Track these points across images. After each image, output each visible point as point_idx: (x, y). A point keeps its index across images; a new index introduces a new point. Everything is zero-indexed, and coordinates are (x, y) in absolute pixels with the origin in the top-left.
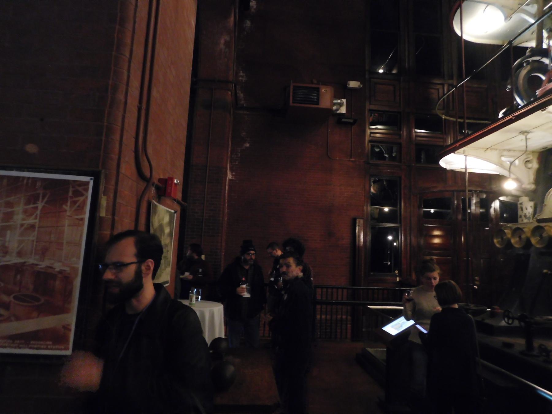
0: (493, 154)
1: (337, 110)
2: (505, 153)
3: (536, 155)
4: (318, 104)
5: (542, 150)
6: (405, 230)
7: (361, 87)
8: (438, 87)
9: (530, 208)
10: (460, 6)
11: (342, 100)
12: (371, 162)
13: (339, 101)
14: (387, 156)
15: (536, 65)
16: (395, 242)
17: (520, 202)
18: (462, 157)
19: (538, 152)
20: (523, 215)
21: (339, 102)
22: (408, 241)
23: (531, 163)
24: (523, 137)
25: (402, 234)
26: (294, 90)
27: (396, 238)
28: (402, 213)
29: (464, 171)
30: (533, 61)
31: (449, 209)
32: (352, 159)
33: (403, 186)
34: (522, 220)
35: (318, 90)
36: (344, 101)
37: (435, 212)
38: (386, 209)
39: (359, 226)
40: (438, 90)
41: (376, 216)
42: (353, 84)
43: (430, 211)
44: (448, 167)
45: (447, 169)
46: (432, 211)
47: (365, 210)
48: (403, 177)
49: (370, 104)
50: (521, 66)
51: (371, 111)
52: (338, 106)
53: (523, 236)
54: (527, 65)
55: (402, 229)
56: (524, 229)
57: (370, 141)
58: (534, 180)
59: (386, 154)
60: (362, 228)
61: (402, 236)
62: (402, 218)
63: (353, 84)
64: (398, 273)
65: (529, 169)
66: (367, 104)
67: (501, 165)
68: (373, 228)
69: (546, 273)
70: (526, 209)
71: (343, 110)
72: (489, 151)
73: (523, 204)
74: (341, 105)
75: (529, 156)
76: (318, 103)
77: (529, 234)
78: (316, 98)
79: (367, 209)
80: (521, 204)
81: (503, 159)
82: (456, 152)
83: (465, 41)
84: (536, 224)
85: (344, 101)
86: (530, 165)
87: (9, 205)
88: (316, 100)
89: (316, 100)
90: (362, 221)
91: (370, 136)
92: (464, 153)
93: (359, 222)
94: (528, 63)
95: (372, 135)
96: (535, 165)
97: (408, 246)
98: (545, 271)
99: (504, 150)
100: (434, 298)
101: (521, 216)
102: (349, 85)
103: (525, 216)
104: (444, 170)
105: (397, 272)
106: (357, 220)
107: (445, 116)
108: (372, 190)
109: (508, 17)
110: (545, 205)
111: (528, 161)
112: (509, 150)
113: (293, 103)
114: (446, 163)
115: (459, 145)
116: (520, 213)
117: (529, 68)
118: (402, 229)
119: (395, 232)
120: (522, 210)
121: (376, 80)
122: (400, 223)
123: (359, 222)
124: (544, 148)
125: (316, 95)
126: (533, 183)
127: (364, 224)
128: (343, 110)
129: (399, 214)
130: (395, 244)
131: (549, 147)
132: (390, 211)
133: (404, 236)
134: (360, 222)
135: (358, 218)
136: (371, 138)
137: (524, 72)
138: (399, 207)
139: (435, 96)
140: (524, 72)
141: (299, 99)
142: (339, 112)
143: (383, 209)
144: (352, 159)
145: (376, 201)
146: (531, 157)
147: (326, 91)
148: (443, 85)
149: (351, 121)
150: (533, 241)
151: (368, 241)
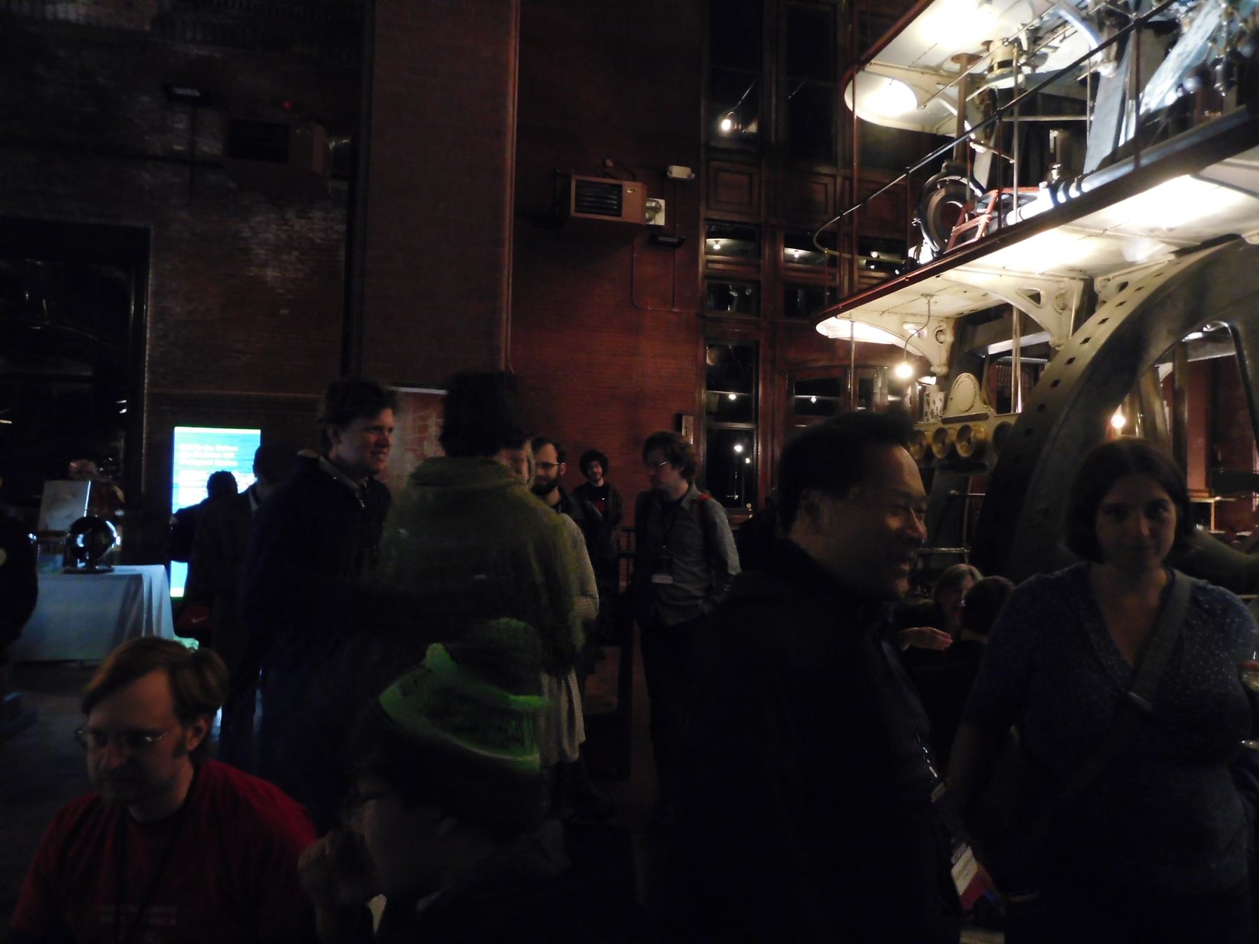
0: (892, 321)
1: (650, 220)
2: (909, 319)
3: (952, 323)
4: (619, 215)
5: (957, 317)
6: (764, 435)
7: (693, 178)
8: (826, 180)
9: (939, 401)
10: (852, 78)
11: (658, 203)
12: (707, 315)
13: (654, 204)
14: (734, 294)
15: (952, 189)
16: (748, 457)
17: (927, 392)
18: (848, 323)
19: (953, 318)
20: (929, 411)
21: (653, 205)
22: (769, 453)
23: (944, 334)
24: (924, 301)
25: (760, 442)
26: (577, 187)
27: (749, 450)
28: (760, 404)
29: (849, 339)
30: (951, 181)
31: (837, 394)
32: (676, 310)
33: (761, 357)
34: (928, 420)
35: (619, 188)
36: (662, 202)
37: (818, 401)
38: (732, 397)
39: (686, 428)
40: (826, 185)
41: (714, 407)
42: (678, 172)
43: (809, 400)
44: (831, 335)
45: (830, 337)
46: (814, 399)
47: (697, 399)
48: (762, 341)
49: (708, 208)
50: (933, 189)
51: (707, 220)
52: (652, 213)
53: (947, 441)
54: (941, 188)
55: (760, 432)
56: (926, 433)
57: (706, 277)
58: (947, 359)
59: (733, 291)
60: (692, 431)
61: (759, 445)
62: (760, 411)
63: (678, 172)
64: (752, 508)
65: (941, 343)
66: (702, 208)
67: (902, 336)
68: (709, 431)
69: (954, 495)
70: (934, 403)
71: (660, 220)
72: (886, 315)
73: (931, 394)
74: (656, 210)
75: (942, 324)
76: (618, 212)
77: (930, 440)
78: (615, 203)
79: (700, 398)
80: (928, 395)
81: (906, 327)
82: (838, 316)
83: (861, 121)
84: (941, 425)
85: (662, 202)
86: (942, 338)
87: (424, 419)
88: (615, 207)
89: (615, 207)
90: (691, 419)
91: (707, 267)
92: (849, 318)
93: (687, 421)
94: (943, 184)
95: (710, 265)
96: (949, 338)
97: (769, 463)
98: (952, 492)
99: (907, 314)
100: (623, 215)
101: (927, 413)
102: (671, 173)
103: (932, 413)
104: (824, 339)
105: (749, 505)
106: (683, 417)
107: (829, 249)
108: (708, 361)
109: (922, 103)
110: (951, 399)
111: (941, 331)
112: (914, 315)
113: (576, 211)
114: (828, 328)
115: (843, 306)
116: (926, 408)
117: (942, 193)
118: (760, 432)
119: (747, 437)
120: (928, 404)
121: (717, 163)
122: (756, 422)
123: (687, 421)
124: (1023, 273)
125: (615, 197)
126: (945, 365)
127: (694, 424)
128: (660, 220)
129: (754, 407)
130: (748, 461)
131: (966, 313)
132: (739, 399)
133: (1188, 407)
134: (688, 421)
135: (686, 415)
136: (708, 271)
137: (936, 198)
138: (754, 391)
139: (820, 197)
140: (936, 198)
141: (587, 204)
142: (652, 223)
143: (726, 396)
144: (676, 310)
145: (716, 381)
146: (944, 326)
147: (634, 191)
148: (834, 177)
149: (675, 240)
150: (935, 449)
151: (702, 454)
